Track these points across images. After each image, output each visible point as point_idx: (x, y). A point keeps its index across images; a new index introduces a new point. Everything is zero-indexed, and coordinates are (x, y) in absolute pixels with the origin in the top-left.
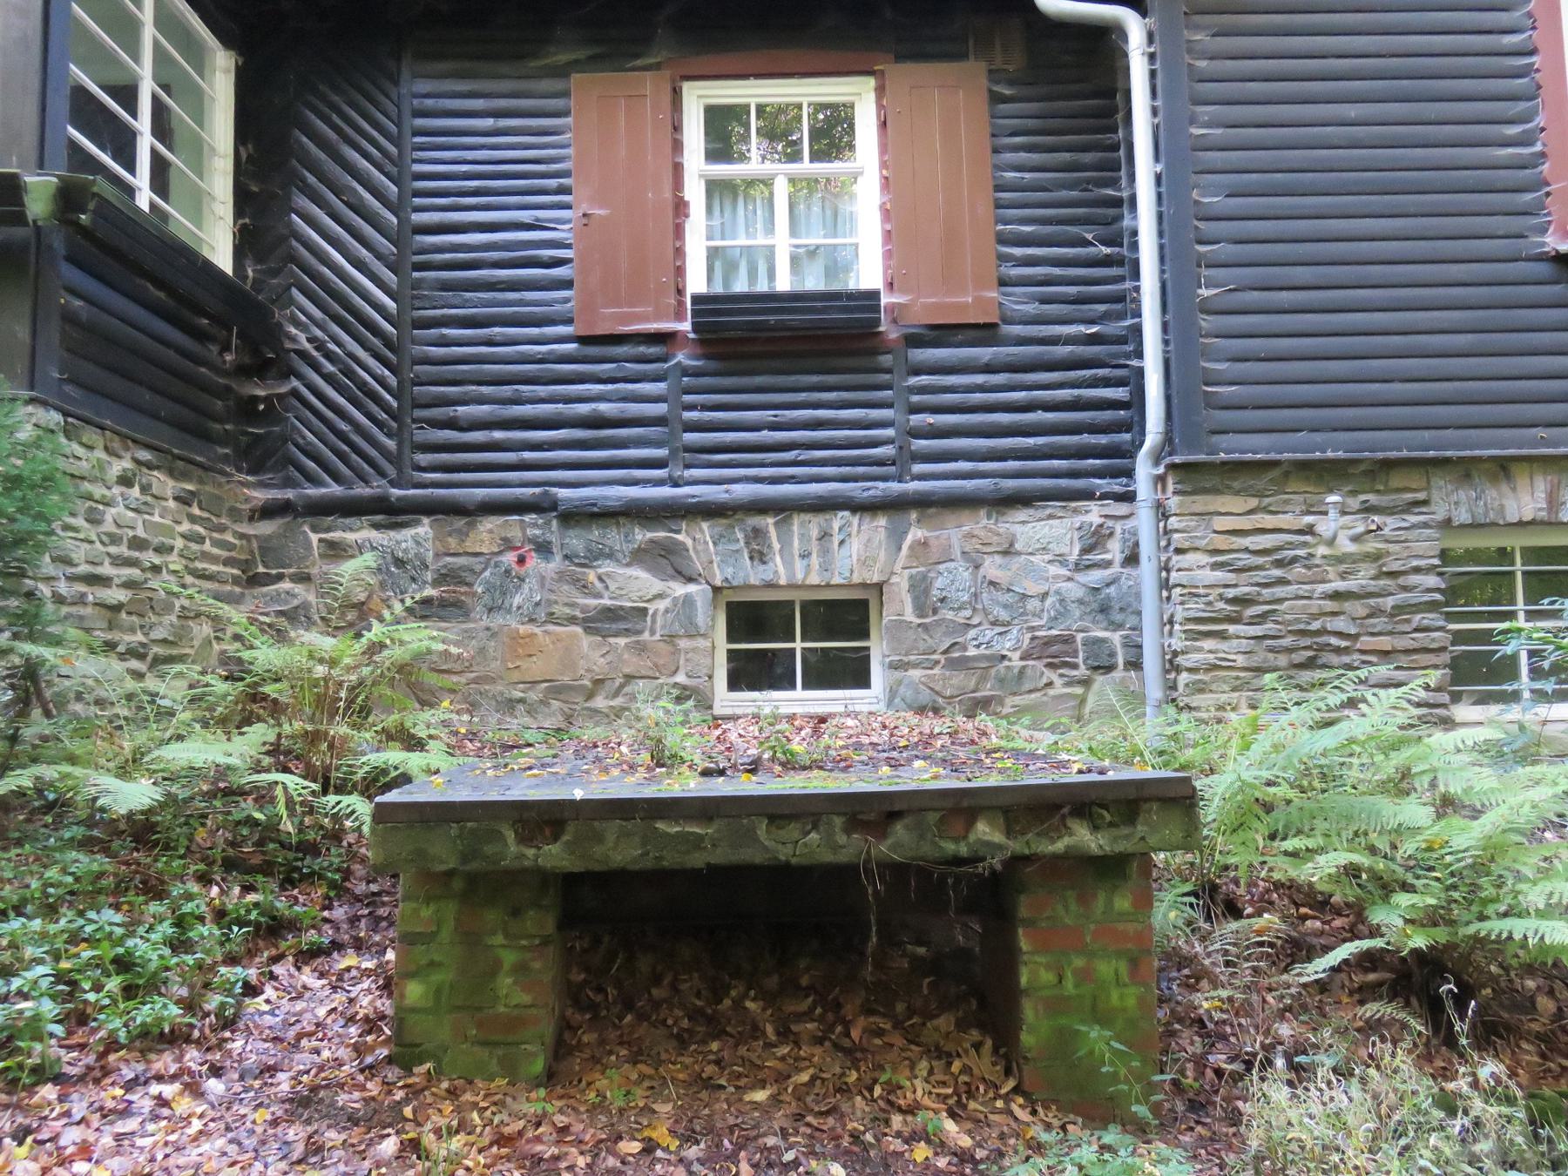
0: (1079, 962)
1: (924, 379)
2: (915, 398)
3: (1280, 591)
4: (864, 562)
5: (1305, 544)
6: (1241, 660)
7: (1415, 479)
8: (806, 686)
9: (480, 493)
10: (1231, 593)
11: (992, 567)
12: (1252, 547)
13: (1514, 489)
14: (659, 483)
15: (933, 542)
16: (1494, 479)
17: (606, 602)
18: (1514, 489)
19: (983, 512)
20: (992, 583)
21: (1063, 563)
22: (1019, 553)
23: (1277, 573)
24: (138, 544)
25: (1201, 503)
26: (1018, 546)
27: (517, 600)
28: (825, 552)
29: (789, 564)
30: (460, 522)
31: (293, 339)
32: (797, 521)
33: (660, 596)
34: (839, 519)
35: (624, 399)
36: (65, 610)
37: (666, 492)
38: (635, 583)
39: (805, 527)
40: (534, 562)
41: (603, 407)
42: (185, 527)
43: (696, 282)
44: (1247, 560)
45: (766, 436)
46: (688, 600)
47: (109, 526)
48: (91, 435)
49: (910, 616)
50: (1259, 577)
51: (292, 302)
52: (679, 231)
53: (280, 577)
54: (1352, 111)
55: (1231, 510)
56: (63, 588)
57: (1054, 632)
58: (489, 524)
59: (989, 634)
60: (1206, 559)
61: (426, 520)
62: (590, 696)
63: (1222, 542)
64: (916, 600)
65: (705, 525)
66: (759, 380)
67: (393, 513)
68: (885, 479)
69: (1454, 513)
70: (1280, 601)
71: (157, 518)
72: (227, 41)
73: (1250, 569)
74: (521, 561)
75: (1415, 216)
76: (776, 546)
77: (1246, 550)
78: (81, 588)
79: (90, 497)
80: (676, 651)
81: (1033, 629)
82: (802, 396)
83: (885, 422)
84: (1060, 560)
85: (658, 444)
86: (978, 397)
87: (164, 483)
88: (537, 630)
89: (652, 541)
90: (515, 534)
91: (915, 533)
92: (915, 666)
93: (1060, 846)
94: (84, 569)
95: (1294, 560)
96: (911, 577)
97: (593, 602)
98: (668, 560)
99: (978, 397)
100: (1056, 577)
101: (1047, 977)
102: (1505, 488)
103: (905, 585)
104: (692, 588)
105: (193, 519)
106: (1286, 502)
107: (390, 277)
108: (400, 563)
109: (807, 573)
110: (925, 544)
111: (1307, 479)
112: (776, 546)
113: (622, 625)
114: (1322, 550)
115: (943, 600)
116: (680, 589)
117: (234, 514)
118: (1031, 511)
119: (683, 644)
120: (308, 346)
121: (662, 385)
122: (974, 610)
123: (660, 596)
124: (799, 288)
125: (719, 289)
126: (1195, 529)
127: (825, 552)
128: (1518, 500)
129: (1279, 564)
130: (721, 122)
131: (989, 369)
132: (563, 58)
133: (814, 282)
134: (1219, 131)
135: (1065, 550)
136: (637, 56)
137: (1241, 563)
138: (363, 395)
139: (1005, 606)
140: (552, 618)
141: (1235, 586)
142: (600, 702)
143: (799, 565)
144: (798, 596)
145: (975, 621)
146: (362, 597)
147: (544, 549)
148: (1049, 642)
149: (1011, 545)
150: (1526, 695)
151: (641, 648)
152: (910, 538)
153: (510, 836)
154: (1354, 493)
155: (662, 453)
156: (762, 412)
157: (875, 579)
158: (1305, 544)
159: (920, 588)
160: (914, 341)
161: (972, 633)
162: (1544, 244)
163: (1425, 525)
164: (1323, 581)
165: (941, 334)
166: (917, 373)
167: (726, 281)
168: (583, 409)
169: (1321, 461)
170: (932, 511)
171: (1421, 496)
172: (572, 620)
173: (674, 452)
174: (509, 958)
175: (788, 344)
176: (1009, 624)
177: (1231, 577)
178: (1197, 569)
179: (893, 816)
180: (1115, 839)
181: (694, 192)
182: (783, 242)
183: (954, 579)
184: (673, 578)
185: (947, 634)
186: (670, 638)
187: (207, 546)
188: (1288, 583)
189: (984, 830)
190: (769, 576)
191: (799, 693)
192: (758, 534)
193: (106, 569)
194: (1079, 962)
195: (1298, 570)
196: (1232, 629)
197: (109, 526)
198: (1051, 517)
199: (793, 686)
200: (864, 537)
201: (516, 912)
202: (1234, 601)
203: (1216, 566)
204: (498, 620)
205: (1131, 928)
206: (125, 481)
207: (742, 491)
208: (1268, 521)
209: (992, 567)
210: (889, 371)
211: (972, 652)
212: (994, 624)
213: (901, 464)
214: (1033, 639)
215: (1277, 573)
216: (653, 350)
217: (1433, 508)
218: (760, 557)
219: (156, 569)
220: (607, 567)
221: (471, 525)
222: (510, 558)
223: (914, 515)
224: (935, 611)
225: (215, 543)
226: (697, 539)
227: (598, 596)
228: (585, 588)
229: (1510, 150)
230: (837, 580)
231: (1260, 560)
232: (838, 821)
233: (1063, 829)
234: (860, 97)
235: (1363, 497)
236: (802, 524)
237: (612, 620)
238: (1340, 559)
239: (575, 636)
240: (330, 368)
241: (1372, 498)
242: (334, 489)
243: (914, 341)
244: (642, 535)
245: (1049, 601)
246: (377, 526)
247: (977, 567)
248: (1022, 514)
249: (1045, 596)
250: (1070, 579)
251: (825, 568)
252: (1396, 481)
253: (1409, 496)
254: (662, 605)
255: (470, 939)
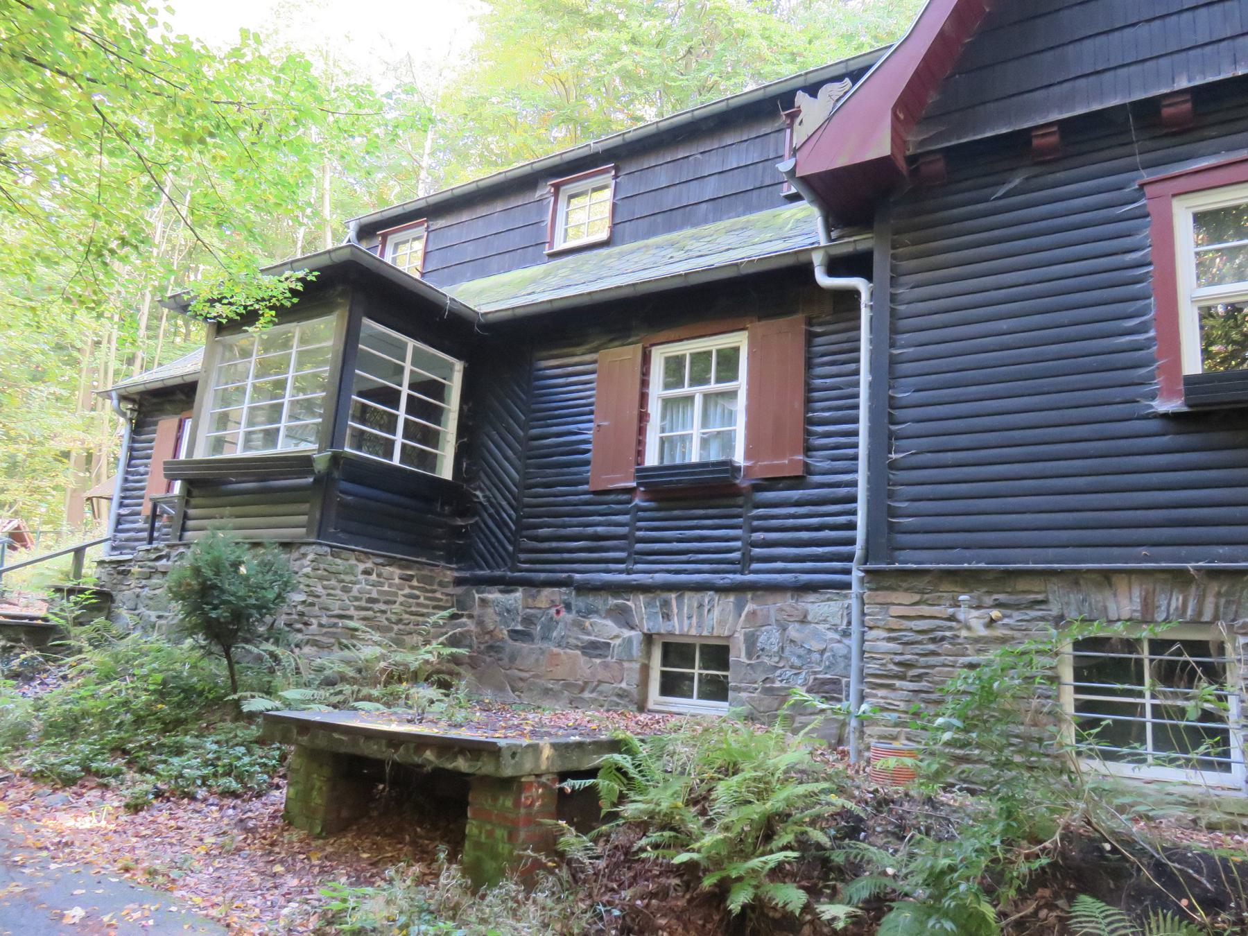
0: (489, 827)
1: (761, 511)
2: (755, 523)
3: (932, 660)
4: (722, 623)
5: (951, 628)
6: (902, 706)
7: (1036, 585)
8: (699, 698)
9: (543, 576)
10: (898, 658)
11: (794, 631)
12: (915, 628)
13: (1115, 595)
14: (621, 572)
15: (759, 613)
16: (1099, 586)
17: (593, 638)
18: (1115, 595)
19: (789, 595)
20: (792, 641)
21: (836, 631)
22: (810, 623)
23: (932, 647)
24: (372, 600)
25: (882, 596)
26: (809, 618)
27: (555, 634)
28: (700, 616)
29: (681, 622)
30: (534, 591)
31: (477, 497)
32: (687, 595)
33: (617, 637)
34: (707, 596)
35: (609, 525)
36: (325, 630)
37: (624, 577)
38: (605, 628)
39: (691, 599)
40: (563, 613)
41: (599, 529)
42: (407, 591)
43: (652, 459)
44: (912, 636)
45: (675, 546)
46: (630, 640)
47: (355, 592)
48: (345, 554)
49: (743, 659)
50: (919, 648)
51: (480, 478)
52: (641, 431)
53: (462, 616)
54: (1004, 325)
55: (902, 602)
56: (324, 620)
57: (828, 676)
58: (547, 592)
59: (789, 673)
60: (886, 635)
61: (521, 589)
62: (582, 690)
63: (894, 624)
64: (747, 648)
65: (641, 597)
66: (676, 513)
67: (508, 585)
68: (734, 572)
69: (1066, 612)
70: (933, 667)
71: (386, 588)
72: (458, 357)
73: (912, 643)
74: (558, 612)
75: (1048, 393)
76: (675, 610)
77: (911, 630)
78: (336, 620)
79: (343, 581)
80: (622, 669)
81: (815, 673)
82: (694, 522)
83: (732, 538)
84: (834, 628)
85: (622, 550)
86: (791, 522)
87: (396, 572)
88: (562, 652)
89: (616, 605)
90: (557, 598)
91: (750, 607)
92: (745, 690)
93: (450, 766)
94: (337, 612)
95: (943, 639)
96: (745, 634)
97: (586, 638)
98: (623, 617)
99: (791, 522)
100: (831, 640)
101: (475, 831)
102: (1108, 593)
103: (742, 638)
104: (633, 633)
105: (412, 587)
106: (939, 597)
107: (517, 462)
108: (508, 611)
109: (690, 626)
110: (754, 613)
111: (956, 582)
112: (675, 610)
113: (599, 652)
114: (964, 633)
115: (763, 650)
116: (627, 633)
117: (441, 584)
118: (817, 595)
119: (626, 665)
120: (482, 499)
121: (628, 517)
122: (781, 658)
123: (617, 637)
124: (705, 460)
125: (666, 463)
126: (878, 614)
127: (700, 616)
128: (1117, 602)
129: (934, 640)
130: (674, 366)
131: (798, 504)
132: (595, 344)
133: (714, 456)
134: (911, 350)
135: (838, 622)
136: (629, 337)
137: (906, 639)
138: (501, 524)
139: (799, 657)
140: (568, 646)
141: (902, 654)
142: (586, 695)
143: (686, 622)
144: (698, 642)
145: (781, 665)
146: (492, 628)
147: (568, 607)
148: (824, 682)
149: (805, 617)
150: (1150, 759)
151: (606, 666)
152: (746, 609)
153: (295, 731)
154: (989, 593)
155: (623, 555)
156: (678, 533)
157: (726, 633)
158: (951, 628)
159: (751, 641)
160: (757, 488)
161: (778, 672)
162: (1152, 407)
163: (1043, 619)
164: (963, 655)
165: (772, 483)
166: (758, 507)
167: (673, 457)
168: (590, 530)
169: (966, 570)
170: (759, 593)
171: (1040, 597)
172: (577, 647)
173: (629, 555)
174: (318, 784)
175: (701, 491)
176: (800, 668)
177: (899, 648)
178: (879, 641)
179: (402, 743)
180: (470, 766)
181: (654, 408)
182: (696, 431)
183: (769, 638)
184: (624, 626)
185: (764, 672)
186: (620, 662)
187: (422, 600)
188: (939, 655)
189: (429, 755)
190: (670, 629)
191: (695, 700)
192: (666, 604)
193: (352, 612)
194: (489, 827)
195: (946, 646)
196: (898, 683)
197: (355, 592)
198: (829, 600)
199: (691, 697)
200: (720, 608)
201: (321, 766)
202: (899, 664)
203: (889, 640)
204: (545, 645)
205: (511, 816)
206: (367, 572)
207: (659, 578)
208: (925, 610)
209: (794, 631)
210: (741, 507)
211: (777, 684)
212: (792, 667)
213: (746, 561)
214: (815, 679)
215: (932, 647)
216: (625, 497)
217: (1051, 606)
218: (667, 617)
219: (384, 612)
220: (595, 619)
221: (539, 592)
222: (553, 611)
223: (749, 596)
224: (758, 657)
225: (426, 598)
226: (637, 604)
227: (589, 634)
228: (583, 630)
229: (1128, 338)
230: (705, 633)
231: (920, 637)
232: (384, 742)
233: (455, 757)
234: (740, 340)
235: (996, 596)
236: (689, 599)
237: (595, 649)
238: (977, 640)
239: (577, 656)
240: (492, 511)
241: (1002, 597)
242: (487, 572)
243: (757, 488)
244: (613, 602)
245: (827, 654)
246: (502, 592)
247: (785, 630)
248: (812, 597)
249: (822, 652)
250: (839, 642)
251: (699, 626)
252: (1022, 585)
253: (1032, 597)
254: (618, 642)
255: (308, 775)
